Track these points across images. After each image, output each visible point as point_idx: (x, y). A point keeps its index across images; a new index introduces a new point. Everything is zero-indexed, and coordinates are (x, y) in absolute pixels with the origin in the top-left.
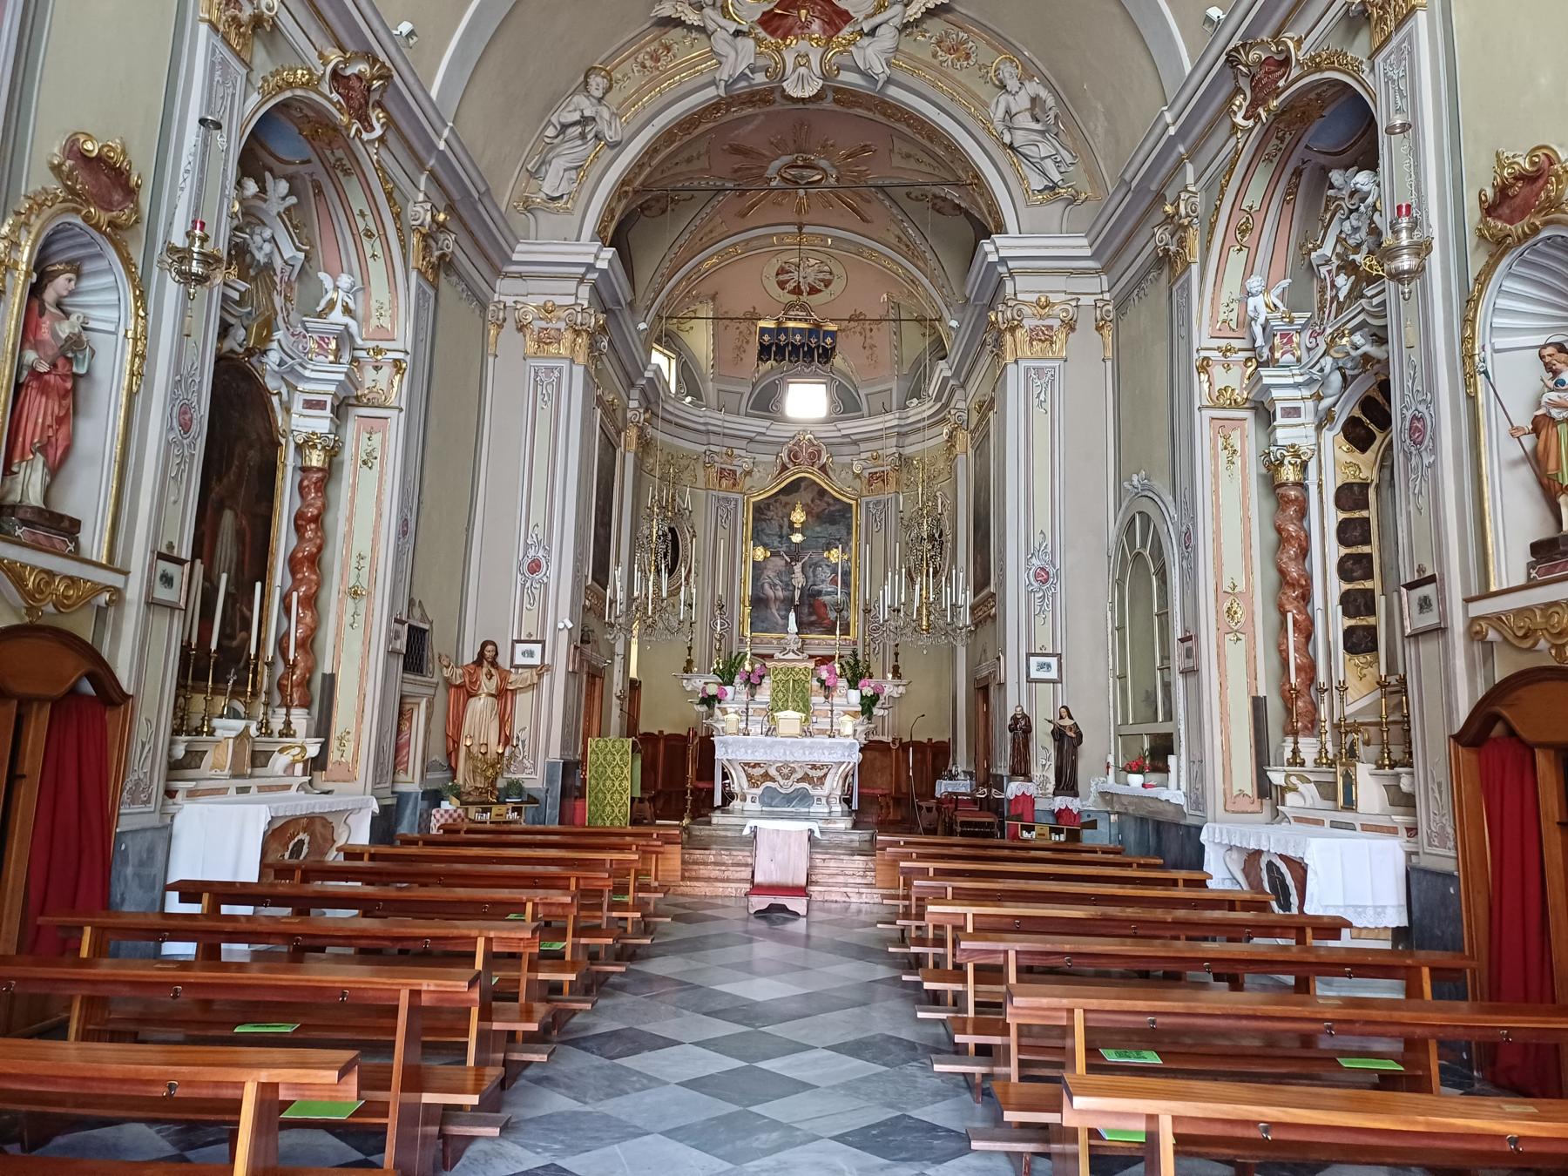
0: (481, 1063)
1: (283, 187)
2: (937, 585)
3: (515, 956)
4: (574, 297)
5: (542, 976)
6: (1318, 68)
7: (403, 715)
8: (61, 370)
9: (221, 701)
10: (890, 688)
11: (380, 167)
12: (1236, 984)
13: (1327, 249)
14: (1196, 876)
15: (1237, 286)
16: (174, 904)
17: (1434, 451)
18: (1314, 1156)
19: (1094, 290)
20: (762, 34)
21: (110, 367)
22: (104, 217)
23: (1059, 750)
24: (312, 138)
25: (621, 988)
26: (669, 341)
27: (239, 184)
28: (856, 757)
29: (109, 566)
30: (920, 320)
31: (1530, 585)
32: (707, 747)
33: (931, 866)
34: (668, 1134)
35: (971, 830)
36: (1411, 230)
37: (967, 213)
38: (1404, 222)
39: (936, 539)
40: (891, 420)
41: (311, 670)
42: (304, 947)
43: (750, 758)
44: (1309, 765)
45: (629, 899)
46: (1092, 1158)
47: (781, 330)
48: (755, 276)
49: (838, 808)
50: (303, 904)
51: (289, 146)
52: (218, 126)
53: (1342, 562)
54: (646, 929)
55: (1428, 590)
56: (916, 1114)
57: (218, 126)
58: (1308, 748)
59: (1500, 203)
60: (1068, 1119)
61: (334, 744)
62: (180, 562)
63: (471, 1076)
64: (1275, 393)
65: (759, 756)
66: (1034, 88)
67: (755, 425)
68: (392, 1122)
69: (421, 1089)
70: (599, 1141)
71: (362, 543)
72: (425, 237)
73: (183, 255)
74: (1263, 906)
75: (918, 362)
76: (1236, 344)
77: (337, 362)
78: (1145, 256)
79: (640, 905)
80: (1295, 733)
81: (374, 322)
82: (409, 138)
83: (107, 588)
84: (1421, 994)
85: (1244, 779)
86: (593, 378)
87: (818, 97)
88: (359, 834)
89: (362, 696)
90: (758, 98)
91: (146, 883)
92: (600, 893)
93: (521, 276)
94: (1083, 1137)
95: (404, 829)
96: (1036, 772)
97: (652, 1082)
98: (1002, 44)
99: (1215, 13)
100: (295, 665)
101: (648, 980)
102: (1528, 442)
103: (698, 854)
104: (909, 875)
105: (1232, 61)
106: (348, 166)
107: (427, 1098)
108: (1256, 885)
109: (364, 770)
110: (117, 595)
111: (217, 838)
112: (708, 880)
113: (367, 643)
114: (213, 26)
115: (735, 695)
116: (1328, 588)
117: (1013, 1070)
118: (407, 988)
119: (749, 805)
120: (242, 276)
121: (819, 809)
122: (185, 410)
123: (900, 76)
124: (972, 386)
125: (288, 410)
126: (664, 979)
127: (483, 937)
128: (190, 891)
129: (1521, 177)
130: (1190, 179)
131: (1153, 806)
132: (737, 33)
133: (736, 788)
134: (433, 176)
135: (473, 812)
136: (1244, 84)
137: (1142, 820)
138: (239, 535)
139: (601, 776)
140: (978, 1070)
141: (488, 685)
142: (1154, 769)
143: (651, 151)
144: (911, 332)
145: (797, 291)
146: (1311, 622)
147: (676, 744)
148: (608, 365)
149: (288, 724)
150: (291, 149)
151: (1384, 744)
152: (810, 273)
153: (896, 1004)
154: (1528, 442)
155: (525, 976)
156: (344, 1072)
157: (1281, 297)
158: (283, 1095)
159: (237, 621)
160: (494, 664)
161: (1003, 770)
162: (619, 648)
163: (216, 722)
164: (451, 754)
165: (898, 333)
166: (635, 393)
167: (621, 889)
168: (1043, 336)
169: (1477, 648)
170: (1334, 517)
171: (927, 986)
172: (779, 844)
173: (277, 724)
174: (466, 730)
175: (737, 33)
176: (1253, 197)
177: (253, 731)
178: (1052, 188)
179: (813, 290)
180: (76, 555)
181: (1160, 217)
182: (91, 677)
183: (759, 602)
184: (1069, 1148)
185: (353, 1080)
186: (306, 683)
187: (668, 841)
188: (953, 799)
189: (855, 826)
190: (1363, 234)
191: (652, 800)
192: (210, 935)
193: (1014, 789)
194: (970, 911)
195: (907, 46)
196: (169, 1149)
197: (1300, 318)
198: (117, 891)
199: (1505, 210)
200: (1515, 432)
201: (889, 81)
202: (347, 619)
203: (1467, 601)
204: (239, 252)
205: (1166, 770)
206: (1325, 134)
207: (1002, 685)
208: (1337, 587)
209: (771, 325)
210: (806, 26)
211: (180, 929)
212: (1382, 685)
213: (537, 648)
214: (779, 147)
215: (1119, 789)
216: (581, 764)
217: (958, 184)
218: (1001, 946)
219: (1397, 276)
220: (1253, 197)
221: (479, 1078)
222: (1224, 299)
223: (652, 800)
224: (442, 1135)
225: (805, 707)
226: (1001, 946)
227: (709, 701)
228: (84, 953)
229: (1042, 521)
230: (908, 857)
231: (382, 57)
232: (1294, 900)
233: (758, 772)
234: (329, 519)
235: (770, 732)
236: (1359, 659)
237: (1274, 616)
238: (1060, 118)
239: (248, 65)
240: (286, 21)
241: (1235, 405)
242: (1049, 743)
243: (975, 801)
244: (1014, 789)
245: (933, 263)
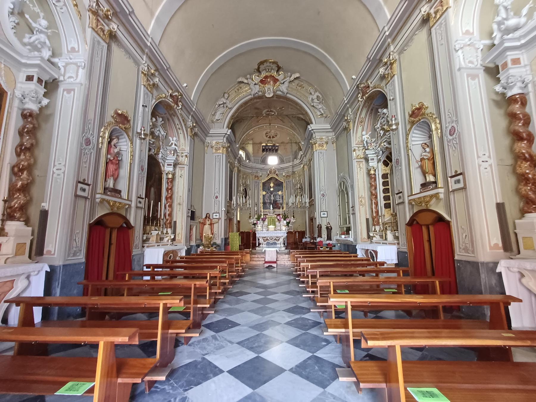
0: (210, 298)
1: (161, 119)
2: (301, 198)
3: (216, 277)
4: (223, 140)
5: (222, 281)
6: (375, 88)
7: (191, 229)
8: (116, 159)
9: (153, 228)
10: (293, 220)
11: (181, 114)
12: (364, 276)
13: (378, 126)
14: (355, 255)
15: (360, 134)
16: (145, 269)
17: (401, 166)
18: (379, 309)
19: (332, 135)
20: (260, 84)
21: (126, 159)
22: (123, 127)
23: (328, 231)
24: (167, 109)
25: (238, 283)
26: (243, 149)
27: (151, 119)
28: (286, 235)
29: (128, 200)
30: (296, 143)
31: (421, 192)
32: (255, 234)
33: (302, 256)
34: (249, 311)
35: (310, 248)
36: (395, 120)
37: (304, 120)
38: (393, 119)
39: (301, 188)
40: (291, 164)
41: (171, 220)
42: (173, 277)
43: (264, 236)
44: (378, 231)
45: (239, 265)
46: (335, 312)
47: (266, 145)
48: (260, 133)
49: (282, 245)
50: (172, 268)
51: (162, 111)
52: (146, 106)
53: (383, 190)
54: (243, 271)
55: (401, 194)
56: (300, 305)
57: (146, 106)
58: (377, 228)
59: (413, 114)
60: (329, 303)
61: (177, 235)
62: (143, 199)
63: (208, 301)
64: (369, 156)
65: (265, 235)
66: (317, 94)
67: (262, 166)
68: (192, 311)
69: (197, 304)
70: (235, 314)
71: (180, 194)
72: (191, 129)
73: (140, 134)
74: (369, 260)
75: (296, 151)
76: (361, 146)
77: (174, 156)
78: (341, 129)
79: (241, 266)
80: (375, 225)
81: (181, 147)
82: (187, 108)
83: (128, 204)
84: (400, 275)
85: (365, 235)
86: (228, 157)
87: (273, 97)
88: (183, 254)
89: (182, 226)
90: (260, 97)
91: (139, 265)
92: (233, 264)
93: (211, 136)
94: (333, 307)
95: (192, 252)
96: (323, 236)
97: (245, 301)
98: (310, 85)
99: (354, 77)
100: (168, 220)
101: (244, 281)
102: (420, 163)
103: (253, 256)
104: (297, 258)
105: (358, 87)
106: (175, 114)
107: (199, 306)
108: (367, 256)
109: (183, 241)
110: (130, 206)
111: (154, 255)
112: (256, 261)
113: (182, 214)
114: (144, 86)
115: (260, 223)
116: (381, 195)
117: (319, 295)
118: (193, 284)
119: (264, 246)
120: (153, 138)
121: (279, 246)
122: (142, 167)
123: (290, 92)
124: (307, 156)
125: (164, 166)
126: (247, 281)
127: (209, 273)
128: (148, 266)
129: (416, 109)
130: (350, 112)
131: (347, 242)
132: (255, 84)
133: (261, 242)
134: (192, 116)
135: (207, 249)
136: (360, 91)
137: (345, 245)
138: (155, 193)
139: (233, 241)
140: (312, 296)
141: (208, 222)
142: (347, 234)
143: (238, 109)
144: (294, 145)
145: (270, 137)
146: (377, 202)
147: (248, 234)
148: (231, 154)
149: (167, 232)
150: (161, 111)
151: (393, 227)
152: (272, 133)
153: (295, 284)
154: (420, 163)
155: (218, 281)
156: (180, 300)
157: (369, 135)
158: (168, 306)
159: (155, 210)
160: (209, 218)
161: (316, 236)
162: (235, 214)
163: (152, 232)
164: (201, 237)
165: (292, 146)
166: (236, 160)
167: (238, 263)
168: (321, 145)
169: (410, 206)
170: (381, 181)
171: (301, 280)
172: (270, 253)
173: (165, 232)
174: (204, 232)
175: (255, 84)
176: (363, 115)
177: (160, 233)
178: (322, 114)
179: (273, 137)
180: (121, 198)
181: (344, 120)
182: (125, 223)
183: (264, 203)
184: (330, 310)
185: (182, 302)
186: (170, 223)
187: (247, 253)
188: (306, 243)
189: (286, 249)
190: (385, 122)
191: (244, 245)
192: (153, 275)
193: (318, 240)
194: (310, 264)
195: (291, 86)
196: (147, 318)
197: (374, 140)
198: (133, 268)
199: (414, 116)
200: (417, 162)
201: (287, 93)
202: (178, 209)
203: (408, 196)
204: (152, 133)
205: (349, 234)
206: (378, 101)
207: (316, 218)
208: (382, 195)
209: (264, 145)
210: (270, 82)
211: (147, 274)
212: (392, 215)
213: (218, 214)
214: (265, 108)
215: (340, 239)
216: (228, 238)
217: (302, 114)
218: (316, 270)
219: (393, 130)
220: (363, 115)
221: (209, 301)
222: (358, 137)
223: (244, 245)
224: (202, 313)
225: (275, 225)
226: (316, 270)
227: (254, 224)
228: (127, 279)
229: (323, 184)
230: (297, 254)
231: (181, 91)
232: (375, 259)
233: (265, 239)
234: (173, 189)
235: (268, 230)
236: (387, 210)
237: (370, 202)
238: (323, 99)
239: (152, 94)
240: (160, 84)
241: (361, 158)
242: (325, 230)
243: (311, 243)
244: (318, 240)
245: (298, 131)
